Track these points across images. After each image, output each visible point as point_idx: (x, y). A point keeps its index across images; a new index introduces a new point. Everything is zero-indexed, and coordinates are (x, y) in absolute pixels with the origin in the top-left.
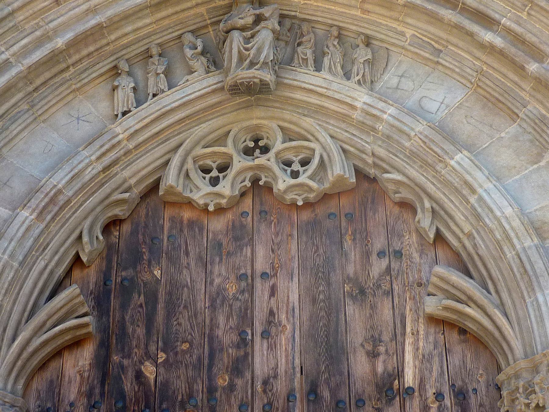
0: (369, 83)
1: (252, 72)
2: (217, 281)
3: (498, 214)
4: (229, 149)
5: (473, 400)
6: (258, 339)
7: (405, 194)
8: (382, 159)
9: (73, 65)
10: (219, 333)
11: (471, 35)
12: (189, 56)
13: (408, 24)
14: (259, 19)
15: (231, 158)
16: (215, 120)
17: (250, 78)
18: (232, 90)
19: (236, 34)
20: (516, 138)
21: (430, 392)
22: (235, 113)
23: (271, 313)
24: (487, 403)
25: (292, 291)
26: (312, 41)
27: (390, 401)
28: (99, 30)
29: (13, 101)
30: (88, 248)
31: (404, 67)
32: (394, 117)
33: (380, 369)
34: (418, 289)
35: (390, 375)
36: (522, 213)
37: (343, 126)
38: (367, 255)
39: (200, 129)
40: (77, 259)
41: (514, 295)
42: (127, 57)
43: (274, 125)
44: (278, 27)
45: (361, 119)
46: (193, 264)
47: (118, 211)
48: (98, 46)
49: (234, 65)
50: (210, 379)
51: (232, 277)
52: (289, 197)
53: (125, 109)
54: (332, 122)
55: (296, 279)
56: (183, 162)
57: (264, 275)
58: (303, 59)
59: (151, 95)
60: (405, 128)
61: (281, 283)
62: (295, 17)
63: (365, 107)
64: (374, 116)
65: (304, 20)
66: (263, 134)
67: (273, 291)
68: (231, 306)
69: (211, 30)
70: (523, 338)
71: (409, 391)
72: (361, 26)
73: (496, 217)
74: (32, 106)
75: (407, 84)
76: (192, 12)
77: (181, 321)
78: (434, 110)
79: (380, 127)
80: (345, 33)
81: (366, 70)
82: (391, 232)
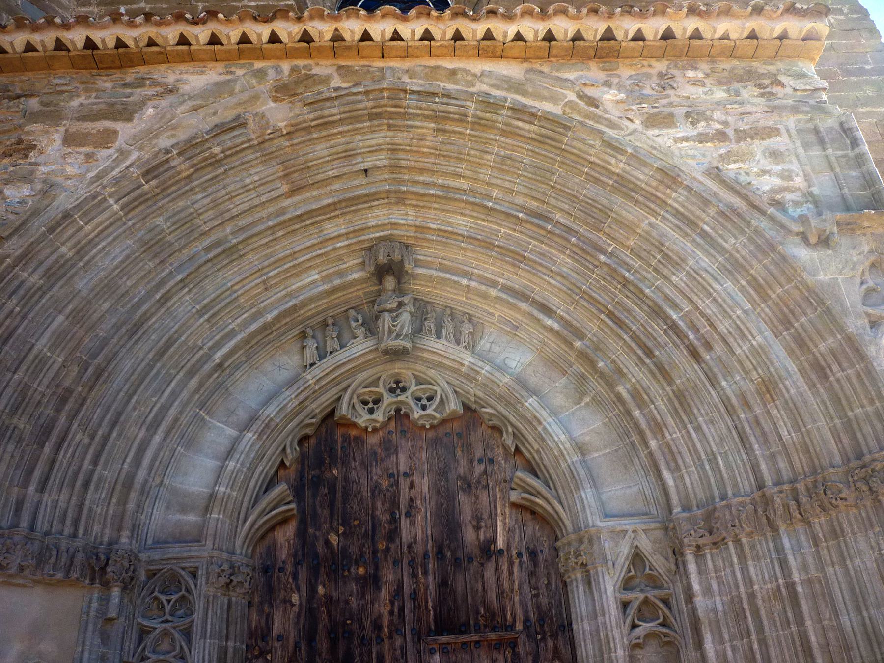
0: (471, 347)
1: (398, 342)
2: (375, 478)
3: (556, 439)
4: (381, 389)
5: (541, 558)
6: (403, 517)
7: (495, 422)
8: (480, 398)
10: (378, 513)
11: (538, 320)
14: (401, 304)
15: (382, 395)
19: (386, 315)
20: (565, 387)
21: (514, 552)
23: (411, 500)
24: (549, 559)
25: (424, 485)
27: (489, 559)
28: (295, 308)
29: (237, 356)
30: (290, 457)
31: (493, 337)
33: (482, 537)
34: (504, 485)
35: (488, 541)
36: (571, 438)
37: (455, 376)
38: (471, 461)
40: (282, 463)
41: (566, 491)
43: (409, 373)
44: (413, 310)
46: (358, 467)
47: (308, 431)
50: (374, 545)
51: (385, 476)
52: (421, 422)
55: (426, 477)
56: (351, 398)
57: (405, 474)
61: (417, 480)
67: (412, 486)
68: (385, 495)
70: (572, 520)
71: (501, 552)
73: (554, 441)
74: (249, 359)
75: (495, 348)
76: (354, 294)
77: (353, 505)
78: (514, 366)
82: (487, 447)
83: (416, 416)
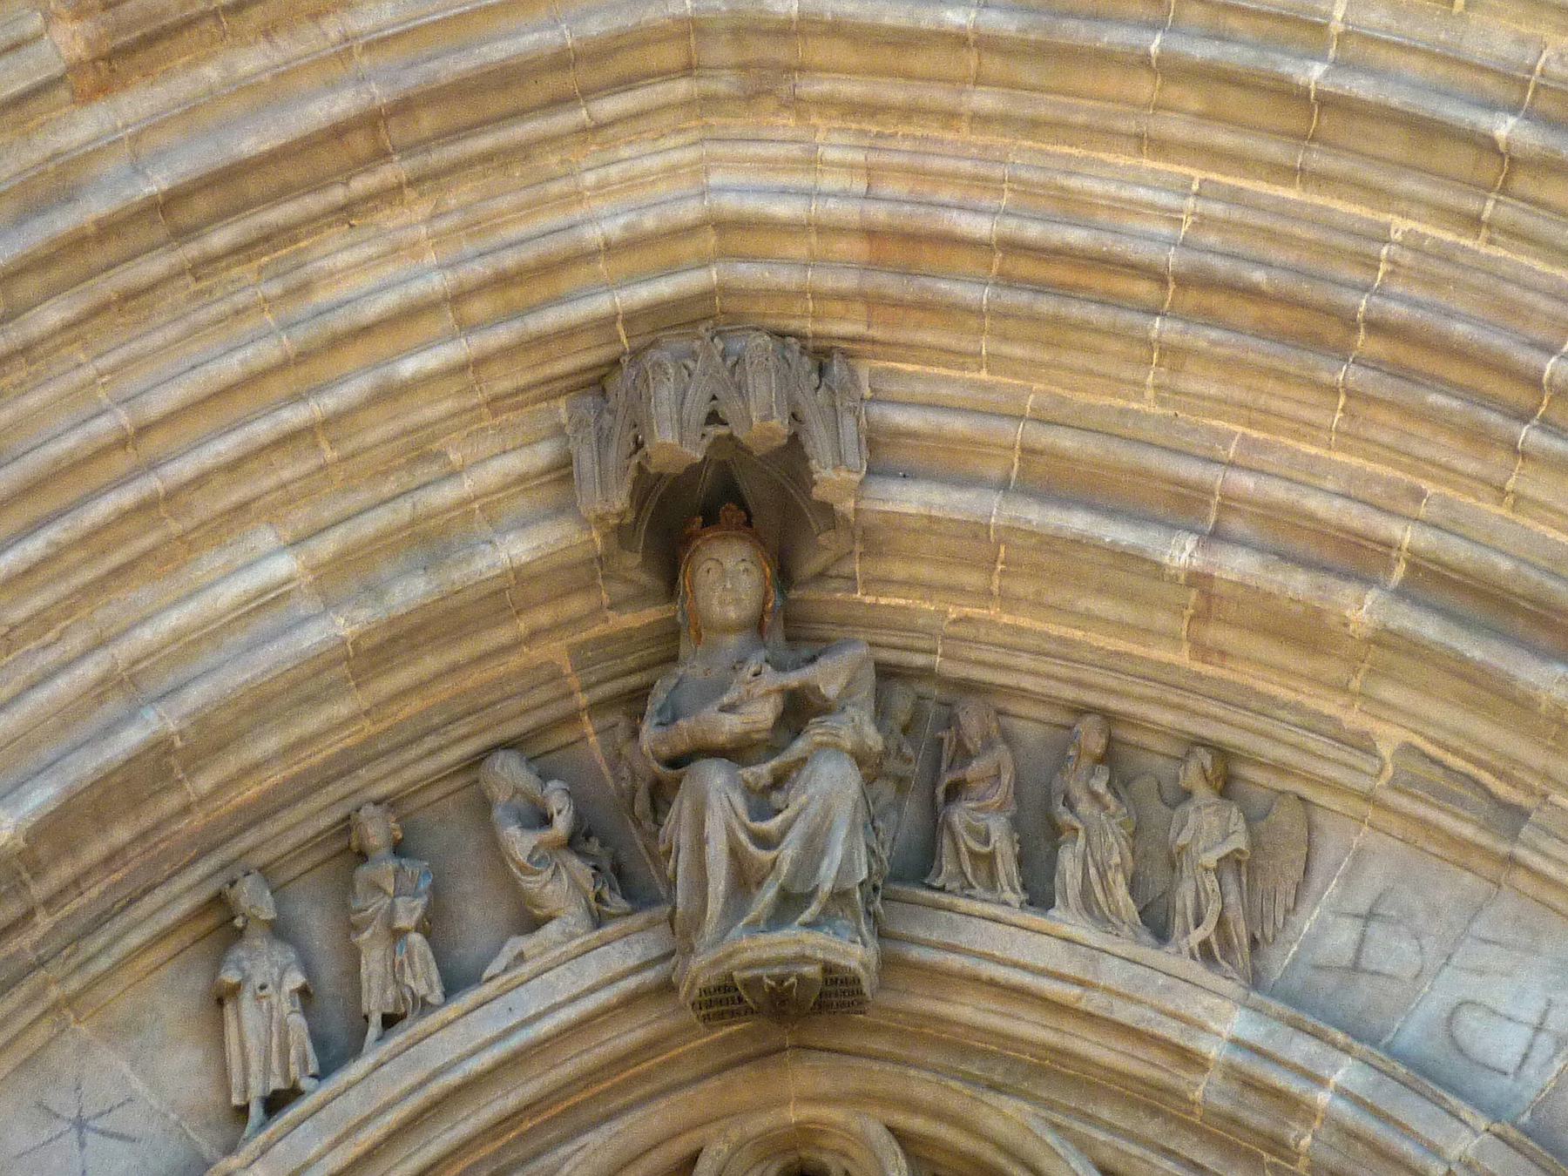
0: (1238, 951)
9: (49, 903)
12: (522, 857)
13: (1384, 704)
14: (799, 710)
16: (639, 1114)
17: (785, 961)
18: (710, 1004)
19: (715, 779)
22: (715, 1083)
26: (1006, 778)
28: (158, 765)
31: (1375, 877)
32: (1357, 1101)
37: (1151, 1128)
39: (579, 1157)
42: (262, 857)
45: (1225, 1105)
48: (146, 821)
49: (715, 906)
53: (277, 1083)
54: (1105, 1113)
58: (973, 855)
59: (376, 1019)
60: (1407, 1147)
62: (926, 673)
63: (1239, 1058)
64: (1277, 1094)
65: (969, 687)
66: (826, 1158)
69: (590, 729)
72: (1194, 713)
75: (1394, 951)
76: (515, 661)
78: (1508, 1056)
79: (1304, 1140)
80: (1133, 736)
81: (1232, 899)
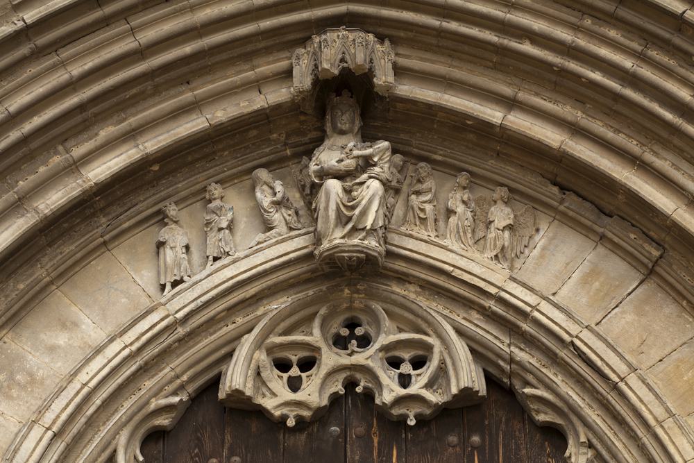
15: (318, 350)
83: (387, 397)
